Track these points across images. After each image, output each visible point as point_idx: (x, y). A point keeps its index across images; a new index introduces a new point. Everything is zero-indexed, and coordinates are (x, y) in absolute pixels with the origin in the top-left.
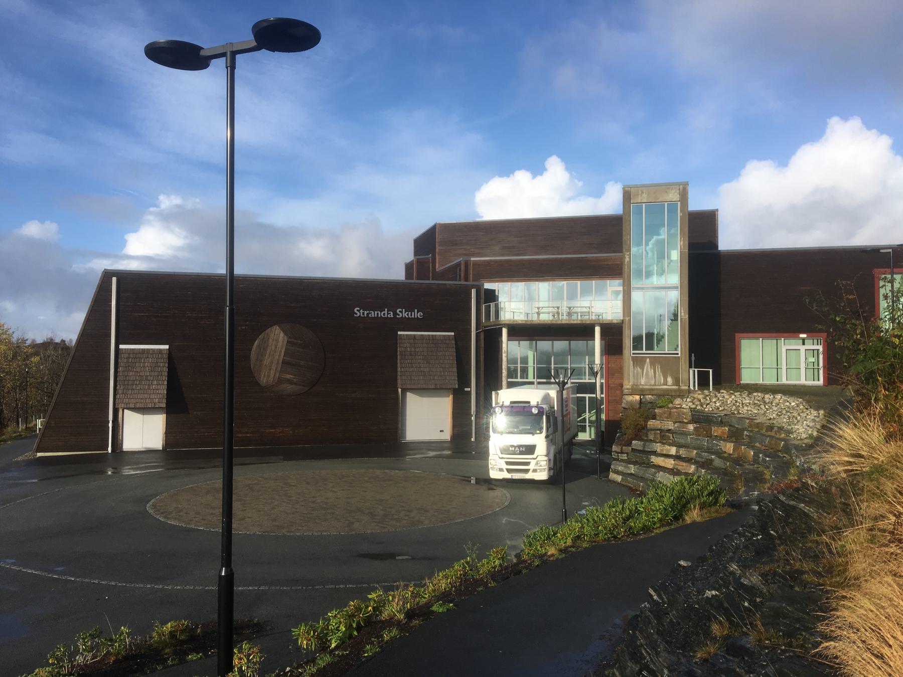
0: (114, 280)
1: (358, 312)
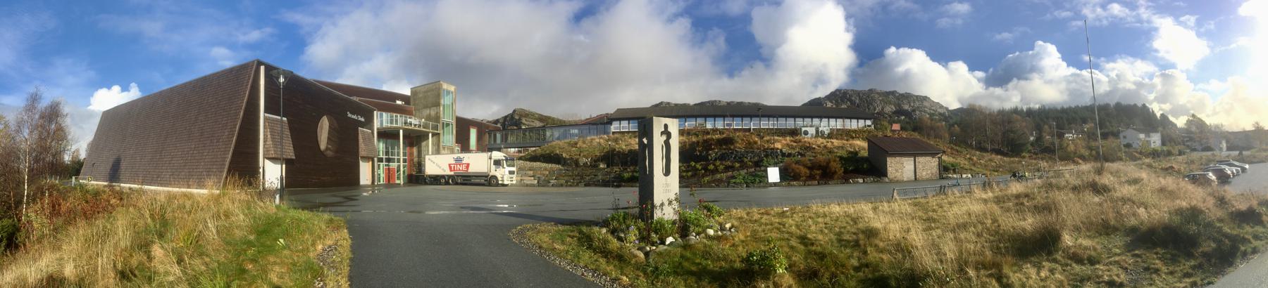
0: (262, 68)
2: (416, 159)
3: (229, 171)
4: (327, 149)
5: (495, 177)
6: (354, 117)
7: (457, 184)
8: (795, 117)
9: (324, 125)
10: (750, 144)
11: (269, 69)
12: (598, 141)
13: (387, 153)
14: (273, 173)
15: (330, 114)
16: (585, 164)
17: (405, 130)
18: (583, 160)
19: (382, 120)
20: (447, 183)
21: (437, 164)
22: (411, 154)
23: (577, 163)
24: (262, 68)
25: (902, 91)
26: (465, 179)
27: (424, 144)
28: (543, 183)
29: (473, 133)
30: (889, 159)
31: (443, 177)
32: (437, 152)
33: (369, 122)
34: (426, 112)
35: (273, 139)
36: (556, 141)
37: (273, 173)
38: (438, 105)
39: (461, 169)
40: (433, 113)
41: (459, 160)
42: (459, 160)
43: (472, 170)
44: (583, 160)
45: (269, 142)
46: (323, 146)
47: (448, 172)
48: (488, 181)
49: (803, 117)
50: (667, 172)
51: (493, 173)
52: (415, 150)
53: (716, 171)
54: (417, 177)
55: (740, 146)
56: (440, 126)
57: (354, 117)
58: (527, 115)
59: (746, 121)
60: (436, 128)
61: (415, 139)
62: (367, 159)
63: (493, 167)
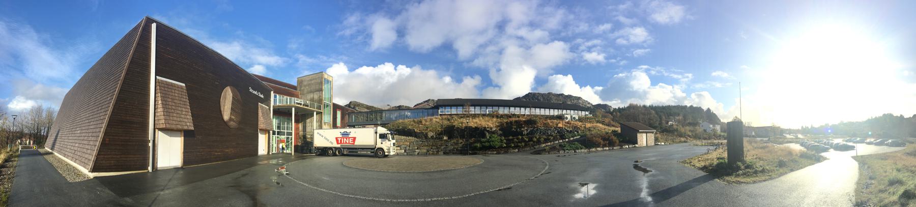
0: (154, 26)
1: (251, 90)
2: (301, 133)
3: (296, 122)
4: (230, 119)
5: (382, 149)
6: (255, 93)
7: (343, 155)
8: (510, 106)
9: (227, 99)
10: (546, 125)
11: (160, 27)
12: (436, 121)
13: (279, 127)
14: (169, 152)
15: (235, 86)
16: (432, 137)
17: (296, 108)
18: (430, 134)
19: (276, 100)
20: (334, 155)
21: (325, 136)
22: (719, 137)
23: (426, 136)
24: (154, 26)
25: (566, 94)
26: (353, 152)
27: (308, 121)
28: (409, 153)
30: (639, 135)
31: (331, 148)
32: (321, 127)
33: (267, 100)
34: (310, 96)
35: (165, 105)
36: (408, 121)
37: (169, 152)
38: (321, 90)
39: (347, 142)
40: (316, 96)
41: (345, 135)
42: (345, 135)
43: (358, 143)
44: (430, 134)
45: (160, 110)
46: (226, 117)
47: (335, 145)
48: (376, 153)
49: (515, 107)
51: (379, 145)
52: (300, 126)
53: (539, 142)
54: (305, 148)
55: (540, 125)
56: (322, 106)
57: (255, 93)
58: (359, 105)
59: (484, 108)
60: (319, 108)
61: (303, 116)
62: (266, 131)
63: (379, 140)
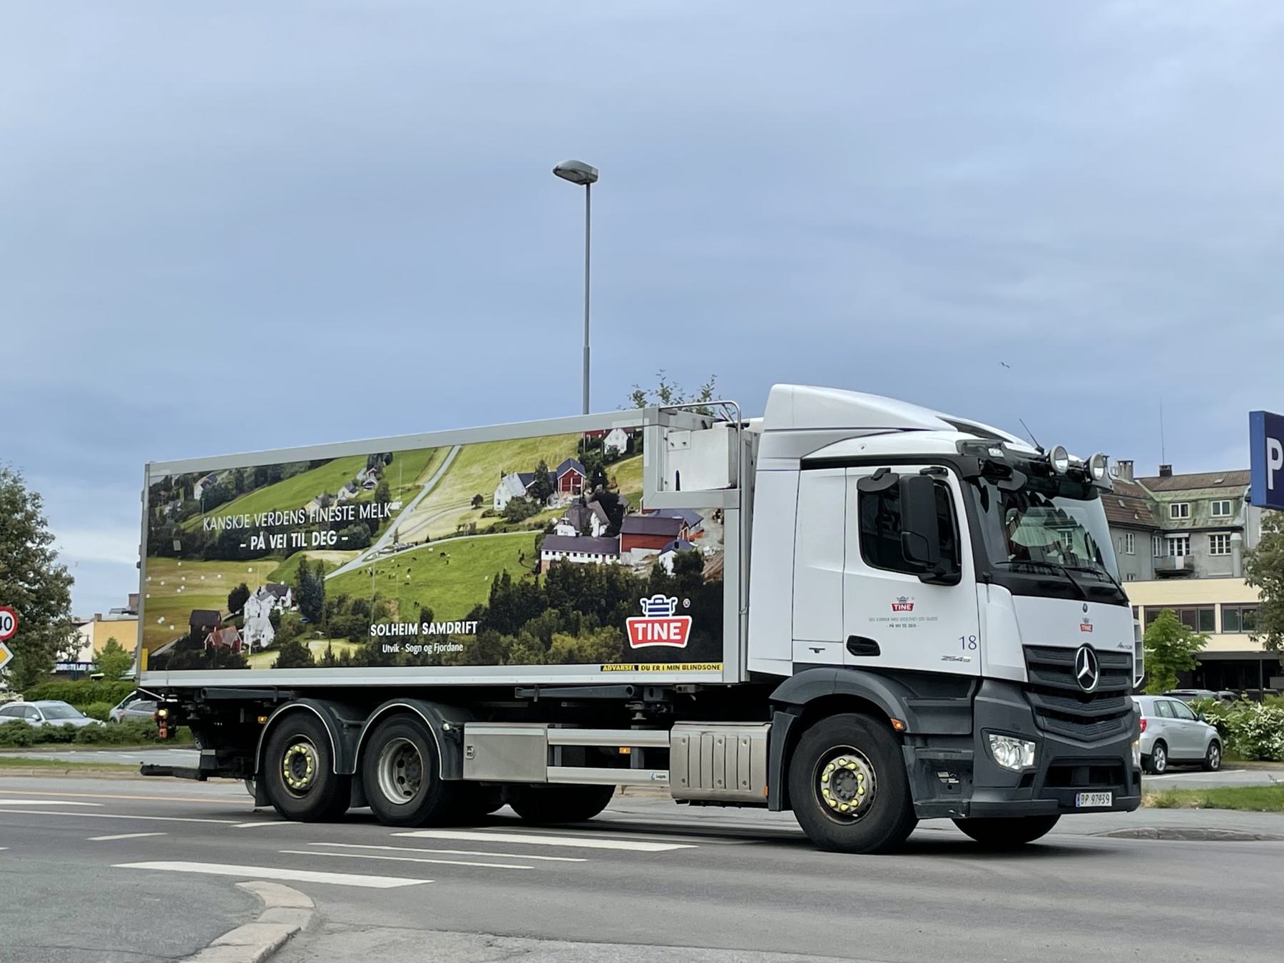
29: (177, 546)
50: (572, 756)
